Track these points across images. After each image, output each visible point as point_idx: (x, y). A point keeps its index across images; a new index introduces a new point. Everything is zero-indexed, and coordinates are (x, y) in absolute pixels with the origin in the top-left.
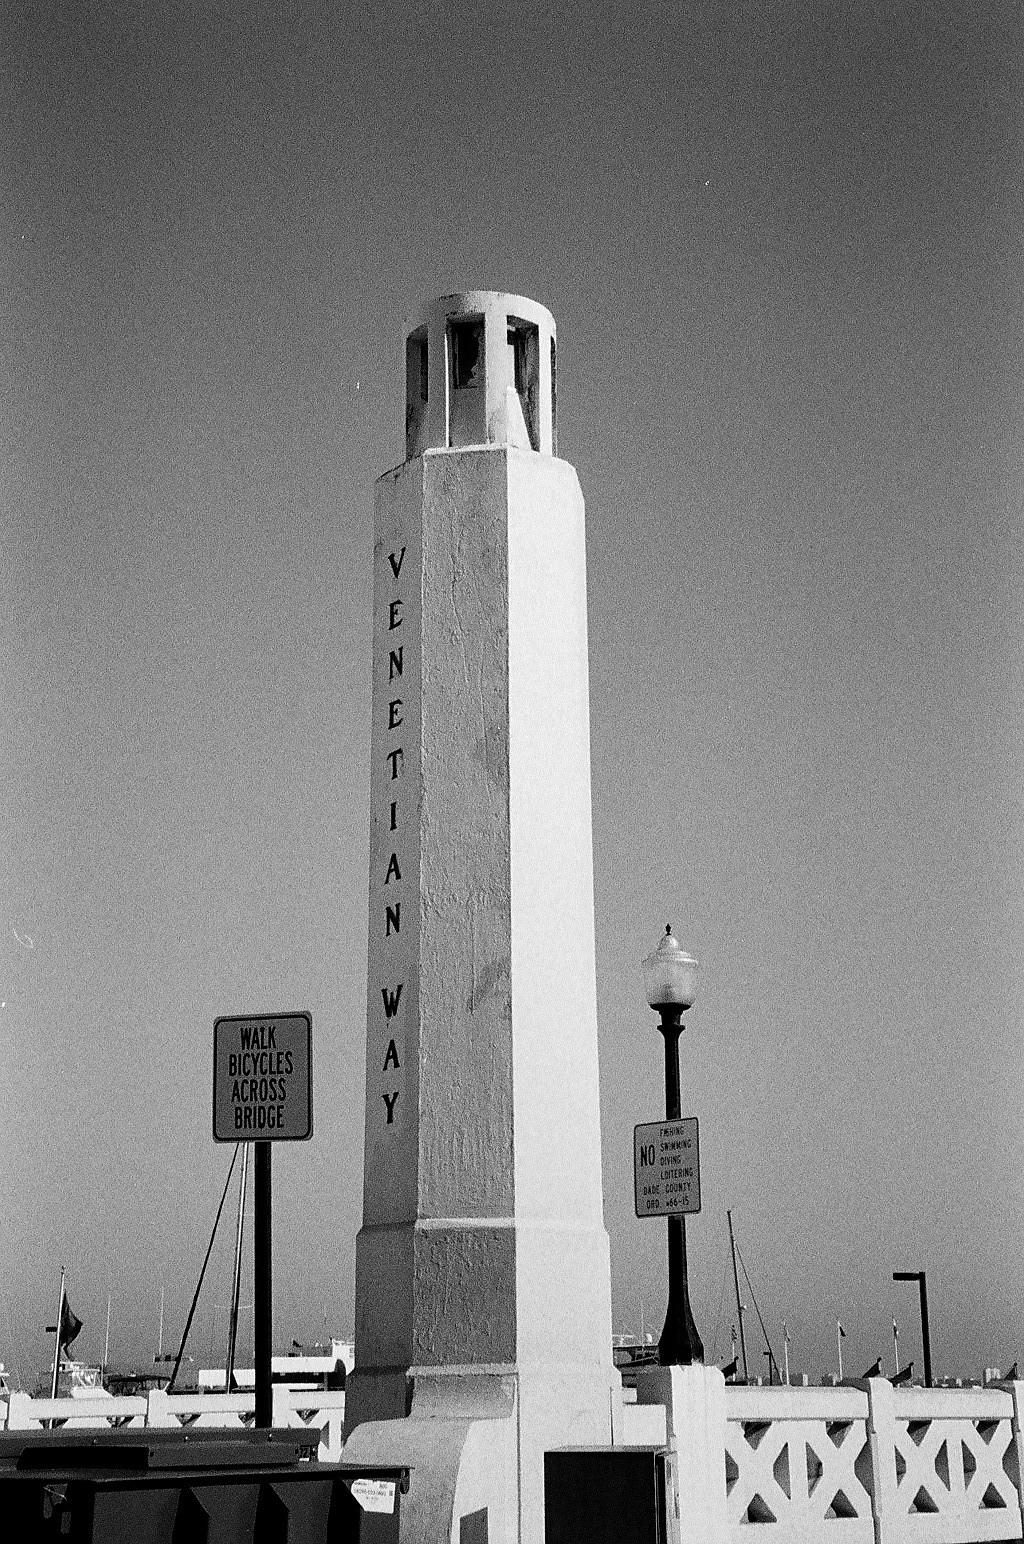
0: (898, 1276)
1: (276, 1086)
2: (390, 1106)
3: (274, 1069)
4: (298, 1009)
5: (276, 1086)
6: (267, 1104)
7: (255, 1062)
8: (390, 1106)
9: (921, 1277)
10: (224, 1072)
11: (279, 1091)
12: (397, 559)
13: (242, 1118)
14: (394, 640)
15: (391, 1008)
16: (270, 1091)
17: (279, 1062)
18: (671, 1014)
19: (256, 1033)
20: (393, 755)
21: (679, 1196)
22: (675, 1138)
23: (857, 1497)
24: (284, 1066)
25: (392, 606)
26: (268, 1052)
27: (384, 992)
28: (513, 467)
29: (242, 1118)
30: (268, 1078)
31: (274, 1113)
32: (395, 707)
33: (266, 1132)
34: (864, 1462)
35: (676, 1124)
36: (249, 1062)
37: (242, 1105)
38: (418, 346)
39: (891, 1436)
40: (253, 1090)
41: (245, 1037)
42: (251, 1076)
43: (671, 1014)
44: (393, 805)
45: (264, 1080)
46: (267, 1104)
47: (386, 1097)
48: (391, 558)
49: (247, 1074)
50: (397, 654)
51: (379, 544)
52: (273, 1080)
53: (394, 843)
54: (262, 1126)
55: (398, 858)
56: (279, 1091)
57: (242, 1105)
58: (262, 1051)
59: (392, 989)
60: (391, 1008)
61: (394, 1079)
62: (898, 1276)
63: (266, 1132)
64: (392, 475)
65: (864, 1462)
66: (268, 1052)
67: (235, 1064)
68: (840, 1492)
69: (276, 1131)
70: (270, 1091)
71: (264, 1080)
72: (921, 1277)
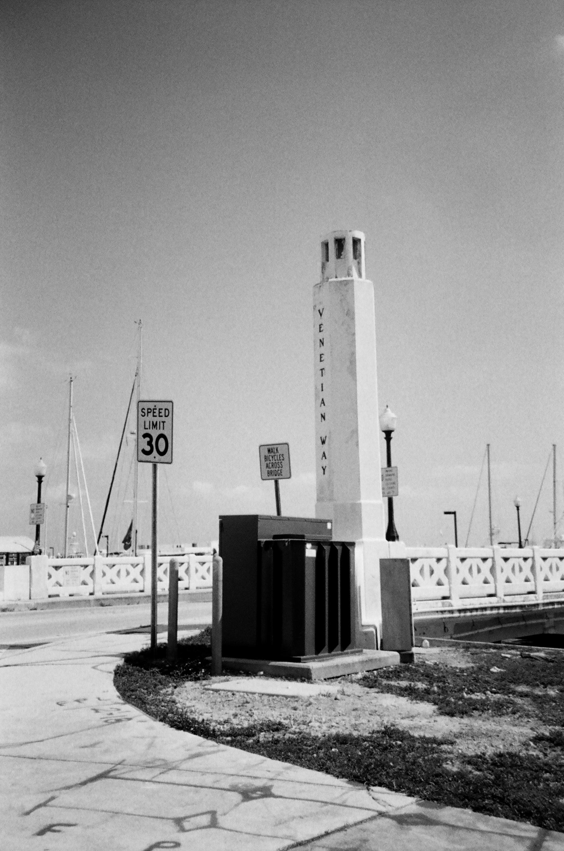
0: (446, 513)
1: (280, 464)
2: (324, 470)
3: (278, 459)
4: (284, 441)
5: (280, 464)
6: (277, 469)
7: (272, 457)
8: (324, 470)
9: (454, 513)
10: (263, 459)
11: (280, 465)
12: (321, 311)
13: (270, 473)
14: (321, 336)
15: (323, 442)
16: (278, 465)
17: (280, 457)
18: (388, 434)
19: (272, 449)
20: (322, 370)
21: (391, 490)
22: (391, 473)
23: (445, 580)
24: (281, 458)
25: (320, 325)
26: (276, 454)
27: (321, 438)
28: (356, 284)
29: (270, 473)
30: (277, 461)
31: (279, 472)
32: (322, 356)
33: (277, 477)
34: (446, 571)
35: (390, 469)
36: (271, 458)
37: (270, 470)
38: (326, 245)
39: (455, 563)
40: (272, 465)
41: (269, 451)
42: (272, 461)
43: (388, 434)
44: (322, 384)
45: (275, 463)
46: (277, 469)
47: (323, 467)
48: (319, 311)
49: (270, 461)
50: (322, 340)
51: (315, 306)
52: (278, 462)
53: (322, 395)
54: (276, 475)
55: (324, 399)
56: (280, 465)
57: (270, 470)
58: (274, 454)
59: (323, 437)
60: (323, 442)
61: (325, 463)
62: (446, 513)
63: (277, 477)
64: (318, 286)
65: (446, 571)
66: (276, 454)
67: (266, 458)
68: (439, 579)
69: (280, 477)
70: (278, 465)
71: (275, 463)
72: (454, 513)
